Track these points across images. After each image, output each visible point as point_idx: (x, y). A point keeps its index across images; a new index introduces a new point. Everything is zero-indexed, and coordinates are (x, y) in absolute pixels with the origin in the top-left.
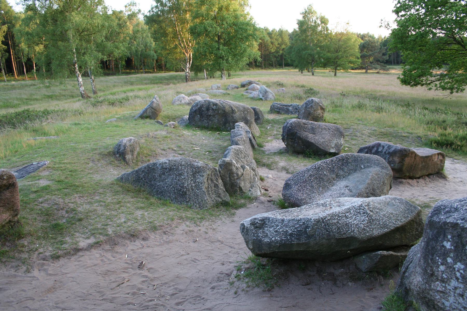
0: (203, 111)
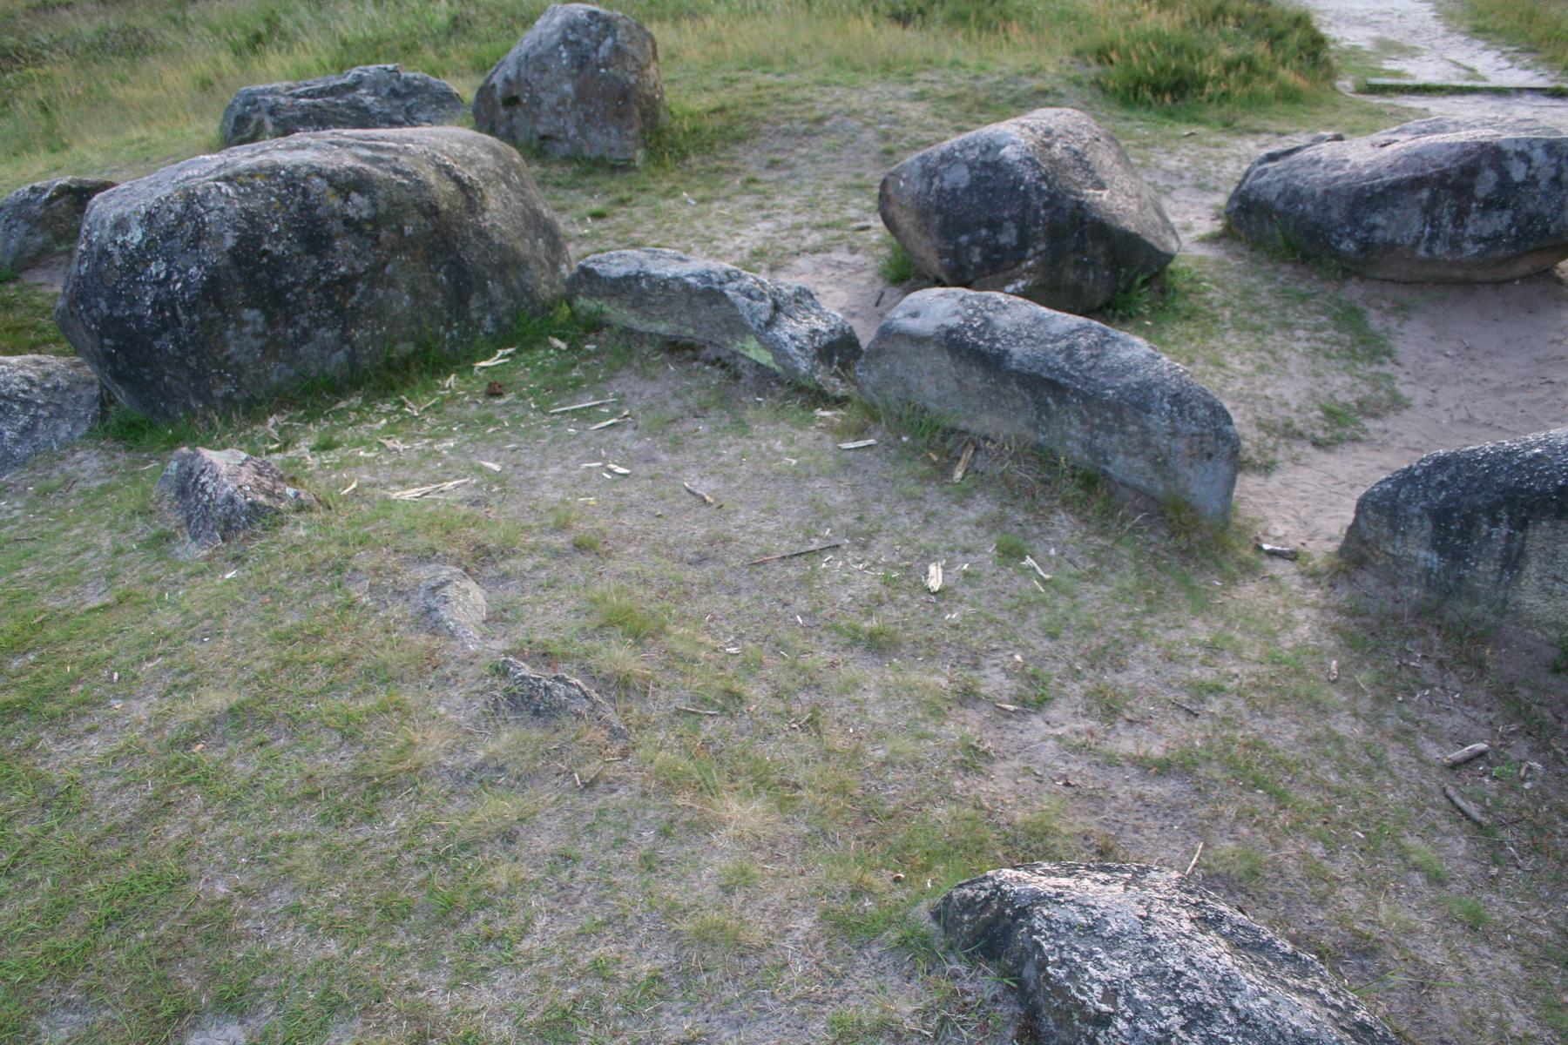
0: (278, 265)
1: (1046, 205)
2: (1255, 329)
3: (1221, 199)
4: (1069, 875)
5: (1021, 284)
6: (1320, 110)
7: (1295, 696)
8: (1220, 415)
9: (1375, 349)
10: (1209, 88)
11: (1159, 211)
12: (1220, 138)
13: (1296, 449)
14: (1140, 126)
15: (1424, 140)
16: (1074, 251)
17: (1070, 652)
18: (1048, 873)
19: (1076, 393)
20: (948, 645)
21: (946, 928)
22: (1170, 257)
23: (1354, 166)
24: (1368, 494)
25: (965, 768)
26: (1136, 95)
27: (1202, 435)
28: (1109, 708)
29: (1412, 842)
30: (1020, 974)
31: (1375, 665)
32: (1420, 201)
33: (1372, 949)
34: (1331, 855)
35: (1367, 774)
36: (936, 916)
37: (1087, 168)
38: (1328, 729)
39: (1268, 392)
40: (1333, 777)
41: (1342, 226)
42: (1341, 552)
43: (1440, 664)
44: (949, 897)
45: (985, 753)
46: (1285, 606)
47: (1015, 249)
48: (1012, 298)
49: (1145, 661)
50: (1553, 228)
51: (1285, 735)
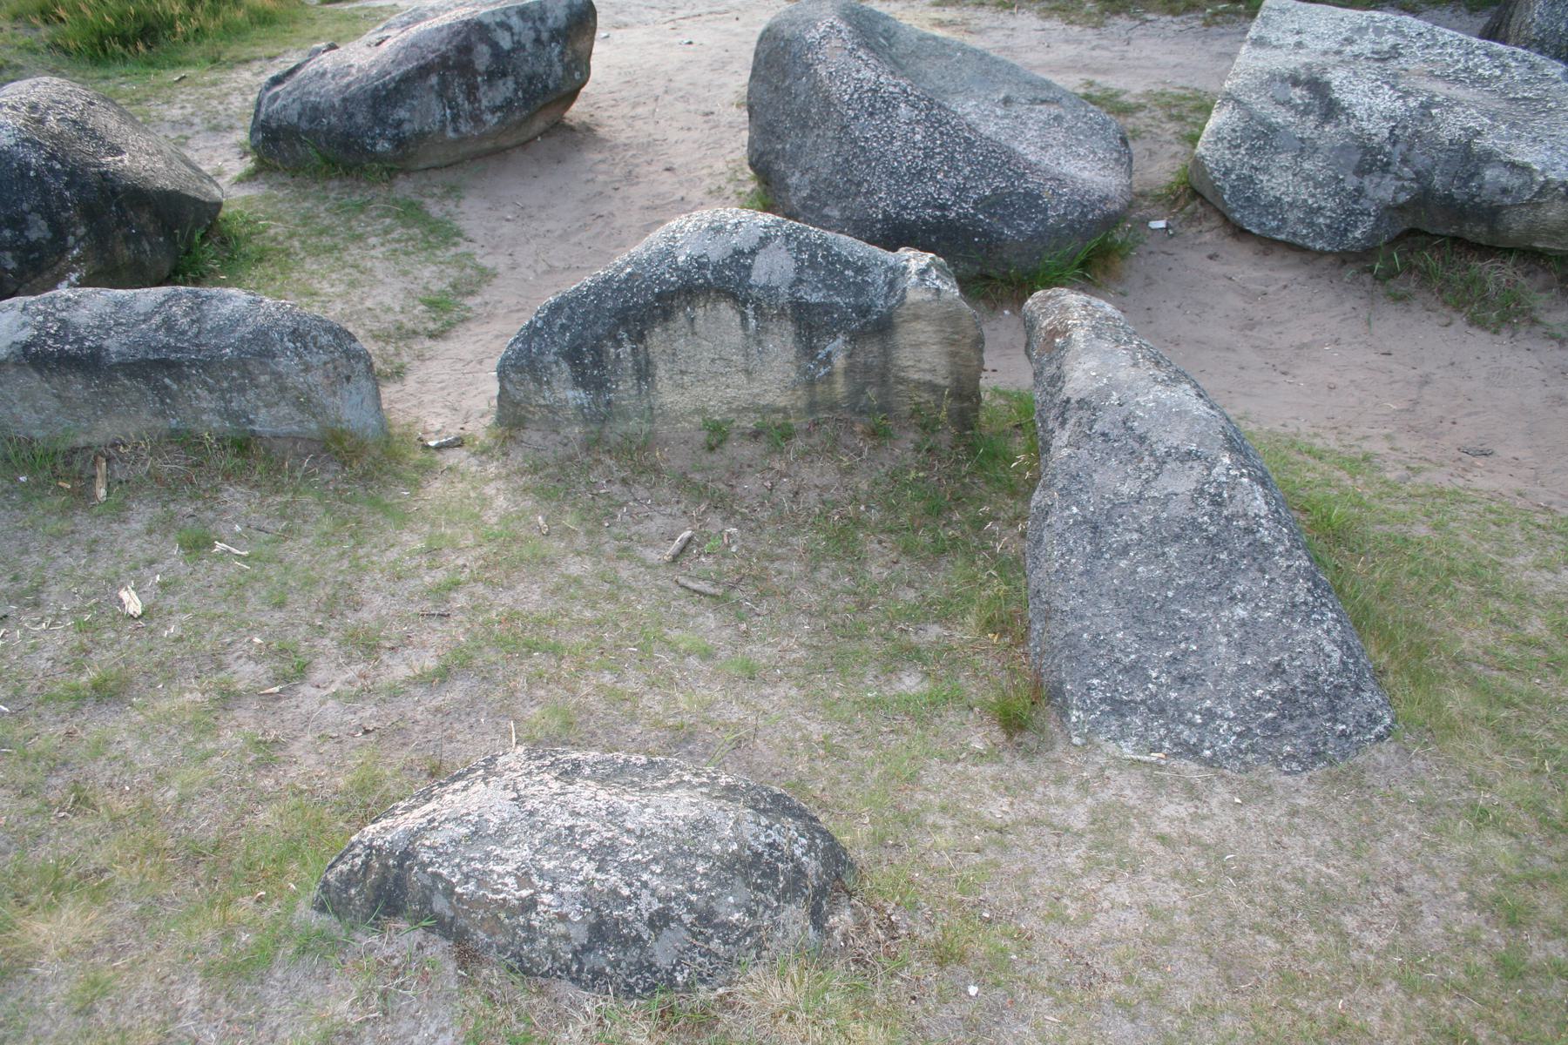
1: (68, 186)
2: (330, 250)
3: (242, 136)
4: (429, 800)
5: (73, 277)
6: (298, 26)
7: (522, 560)
8: (341, 335)
9: (444, 234)
10: (180, 27)
11: (187, 162)
12: (214, 76)
13: (417, 347)
14: (125, 82)
15: (414, 30)
16: (118, 227)
17: (303, 613)
18: (409, 809)
19: (192, 364)
20: (182, 660)
21: (337, 913)
22: (218, 205)
23: (360, 69)
24: (503, 360)
25: (265, 765)
26: (105, 51)
27: (334, 360)
28: (367, 645)
29: (674, 634)
30: (432, 911)
31: (574, 505)
32: (432, 87)
33: (691, 734)
34: (620, 677)
35: (613, 598)
36: (321, 908)
37: (93, 135)
38: (563, 575)
39: (369, 303)
40: (588, 614)
41: (371, 129)
42: (500, 420)
43: (624, 481)
44: (326, 883)
45: (276, 741)
46: (474, 488)
47: (51, 241)
48: (81, 290)
49: (377, 590)
50: (551, 84)
51: (530, 596)
